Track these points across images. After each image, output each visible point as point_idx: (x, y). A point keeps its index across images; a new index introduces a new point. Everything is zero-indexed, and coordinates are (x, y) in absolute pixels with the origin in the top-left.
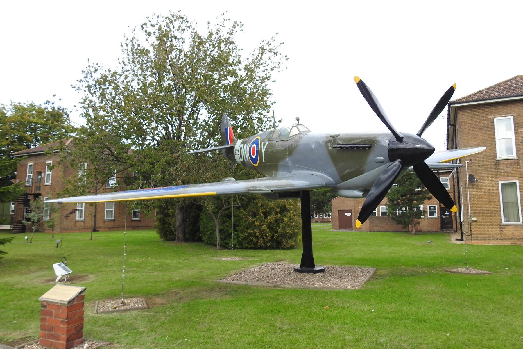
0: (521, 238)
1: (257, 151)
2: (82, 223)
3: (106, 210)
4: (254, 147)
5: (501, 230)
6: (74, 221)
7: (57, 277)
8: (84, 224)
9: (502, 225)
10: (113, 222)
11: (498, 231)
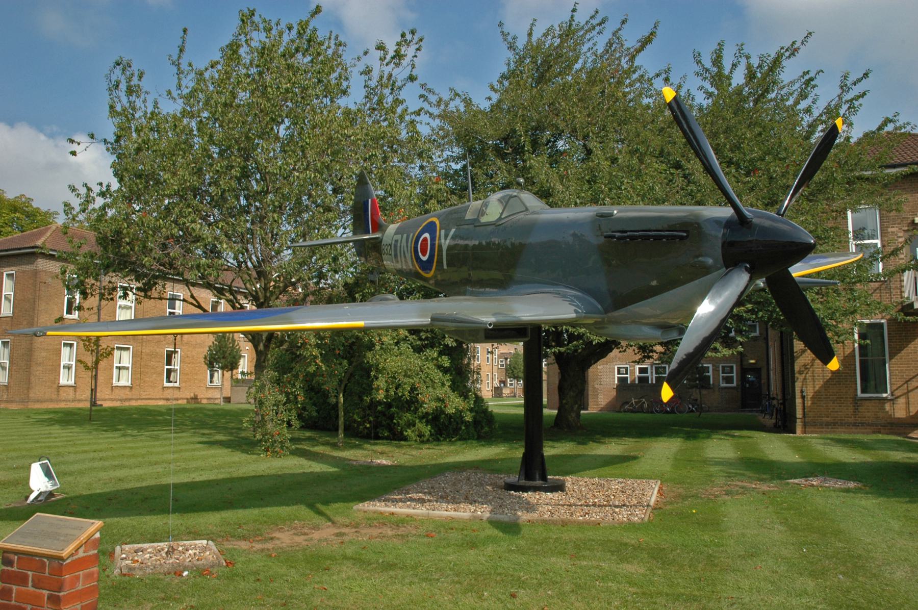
0: (889, 423)
1: (433, 245)
2: (71, 391)
3: (30, 573)
4: (425, 239)
5: (856, 409)
6: (56, 386)
7: (32, 491)
8: (75, 391)
9: (858, 400)
10: (128, 389)
11: (851, 409)
